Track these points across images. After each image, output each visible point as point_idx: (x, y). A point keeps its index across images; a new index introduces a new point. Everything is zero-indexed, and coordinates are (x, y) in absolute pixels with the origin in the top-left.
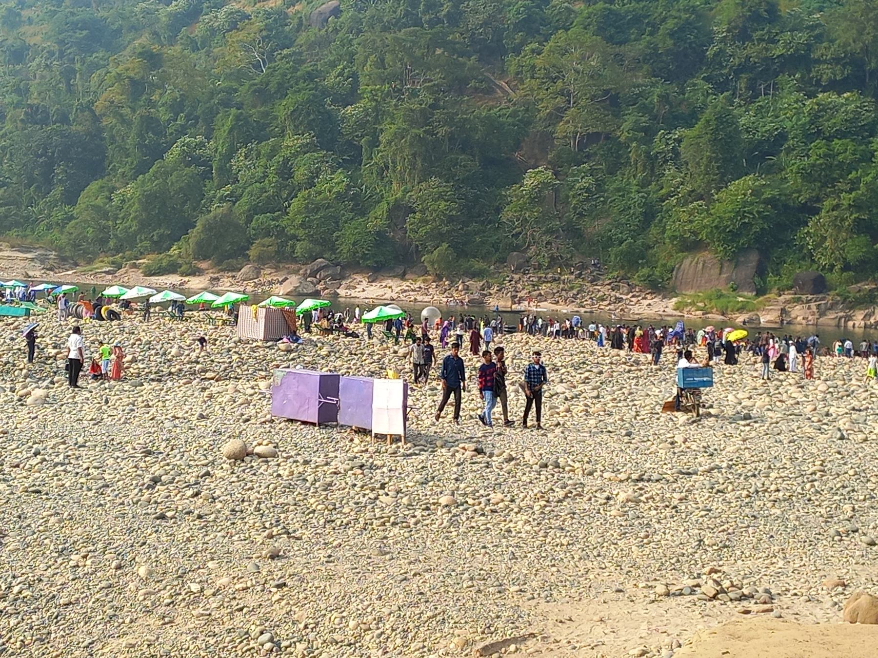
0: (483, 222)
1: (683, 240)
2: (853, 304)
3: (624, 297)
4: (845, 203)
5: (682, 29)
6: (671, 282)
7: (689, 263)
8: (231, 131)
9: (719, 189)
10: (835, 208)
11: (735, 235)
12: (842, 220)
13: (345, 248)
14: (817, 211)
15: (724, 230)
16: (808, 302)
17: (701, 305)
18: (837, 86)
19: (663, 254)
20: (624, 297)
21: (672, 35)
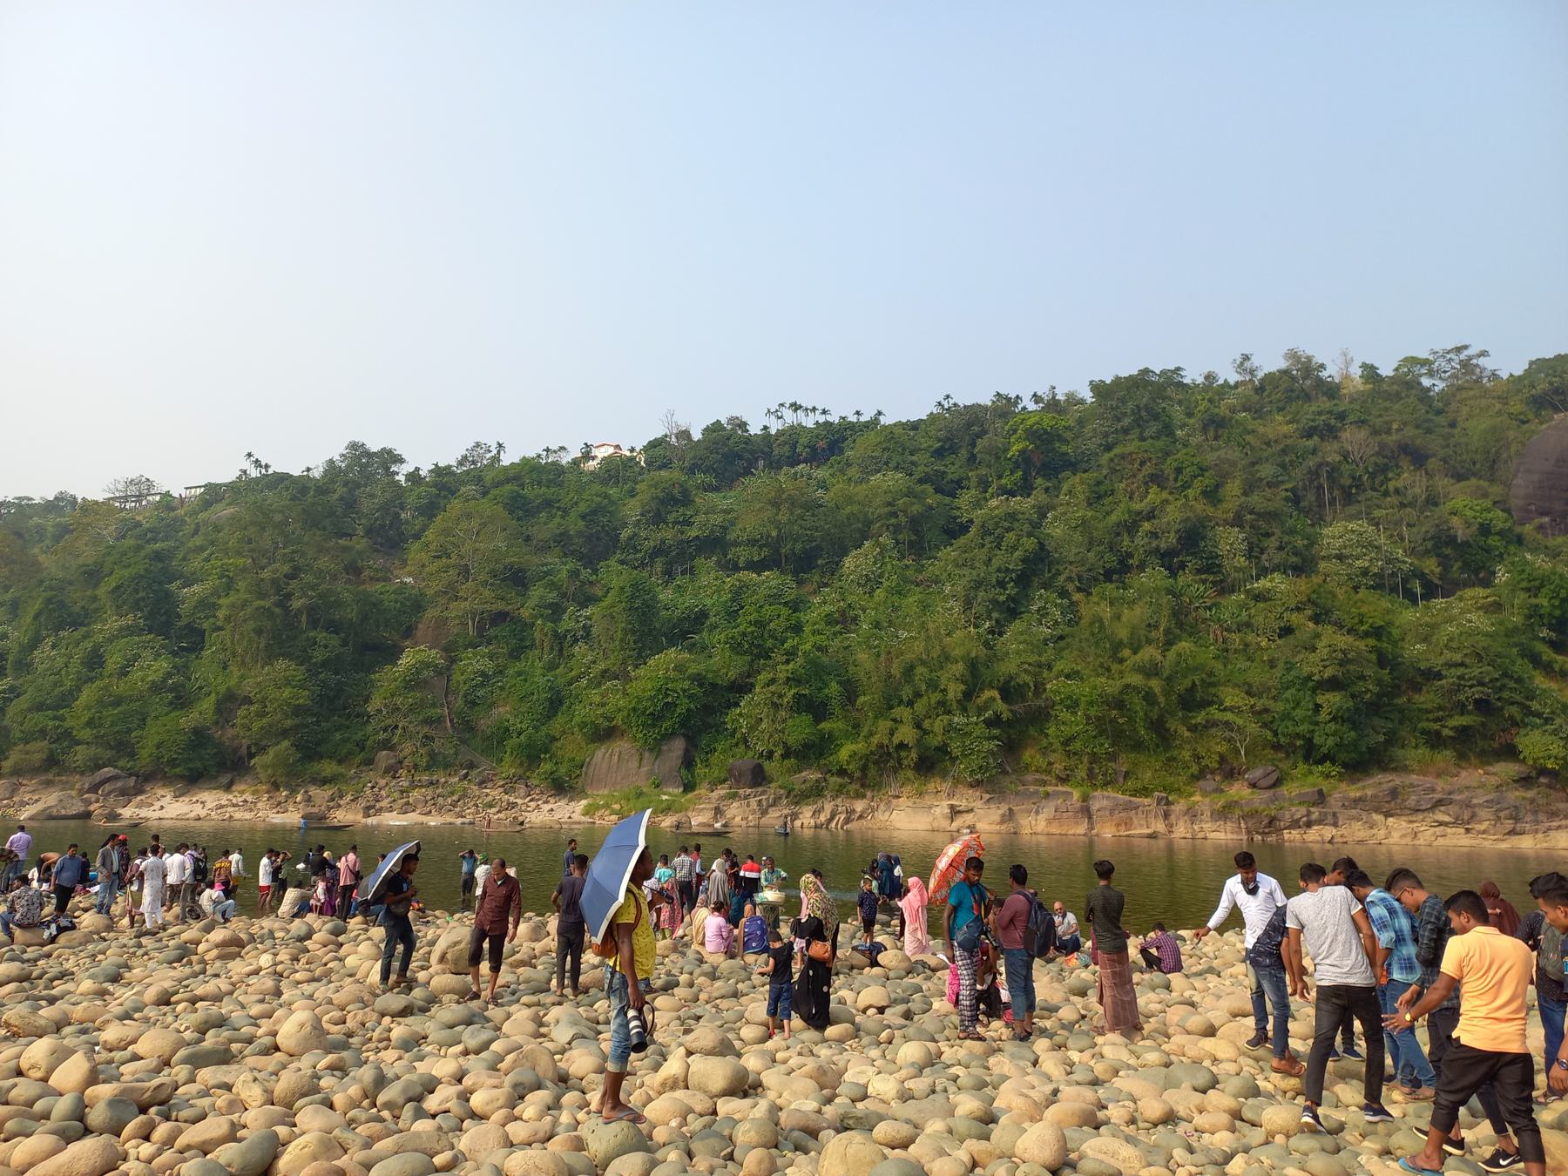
0: (349, 715)
1: (596, 727)
2: (800, 797)
3: (519, 801)
4: (783, 676)
5: (594, 512)
6: (581, 780)
7: (602, 756)
8: (36, 617)
9: (636, 667)
10: (772, 681)
11: (656, 718)
12: (780, 696)
13: (146, 753)
14: (749, 688)
15: (643, 713)
16: (746, 797)
17: (617, 807)
18: (758, 567)
19: (571, 747)
20: (519, 801)
21: (583, 517)
